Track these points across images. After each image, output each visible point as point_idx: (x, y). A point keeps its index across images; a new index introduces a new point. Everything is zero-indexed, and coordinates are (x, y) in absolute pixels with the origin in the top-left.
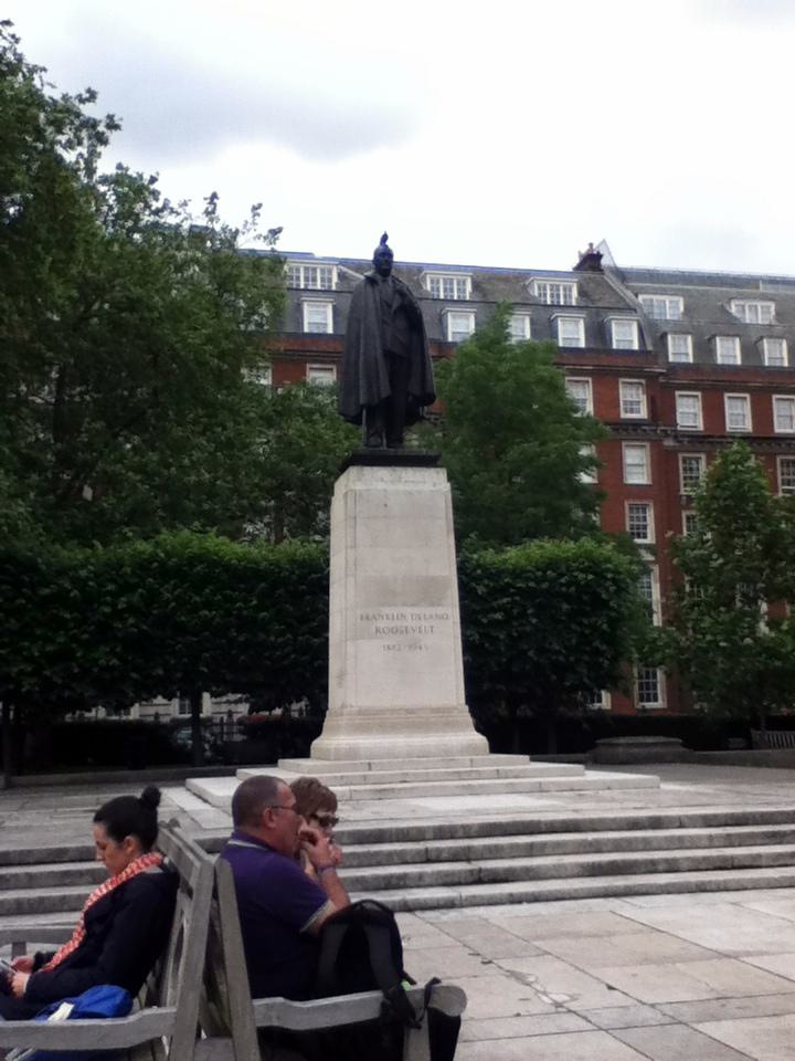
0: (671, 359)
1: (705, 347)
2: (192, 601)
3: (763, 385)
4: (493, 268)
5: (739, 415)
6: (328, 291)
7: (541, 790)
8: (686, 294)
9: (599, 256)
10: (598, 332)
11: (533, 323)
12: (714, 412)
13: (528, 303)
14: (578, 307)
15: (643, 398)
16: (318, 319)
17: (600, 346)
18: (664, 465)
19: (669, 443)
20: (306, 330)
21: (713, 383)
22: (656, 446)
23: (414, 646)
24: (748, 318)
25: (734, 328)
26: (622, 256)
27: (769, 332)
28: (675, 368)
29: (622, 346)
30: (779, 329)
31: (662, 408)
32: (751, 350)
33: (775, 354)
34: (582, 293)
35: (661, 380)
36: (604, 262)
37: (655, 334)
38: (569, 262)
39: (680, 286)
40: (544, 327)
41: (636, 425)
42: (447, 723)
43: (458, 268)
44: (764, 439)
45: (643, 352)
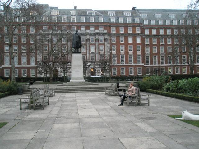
0: (144, 24)
1: (150, 22)
2: (136, 80)
3: (193, 27)
4: (62, 9)
5: (191, 32)
6: (113, 16)
7: (93, 85)
8: (176, 14)
9: (135, 8)
10: (134, 20)
11: (123, 19)
12: (151, 32)
13: (123, 16)
14: (115, 16)
15: (140, 30)
16: (113, 20)
17: (133, 22)
18: (143, 40)
19: (144, 37)
20: (111, 22)
21: (151, 27)
22: (142, 37)
23: (78, 71)
24: (157, 17)
25: (155, 19)
26: (137, 8)
27: (160, 19)
28: (144, 25)
29: (101, 22)
30: (161, 19)
31: (143, 32)
32: (157, 22)
33: (196, 23)
34: (132, 14)
35: (143, 27)
36: (136, 8)
37: (142, 20)
38: (131, 9)
39: (161, 12)
40: (157, 22)
41: (138, 34)
42: (81, 79)
43: (111, 11)
44: (194, 36)
45: (140, 23)
